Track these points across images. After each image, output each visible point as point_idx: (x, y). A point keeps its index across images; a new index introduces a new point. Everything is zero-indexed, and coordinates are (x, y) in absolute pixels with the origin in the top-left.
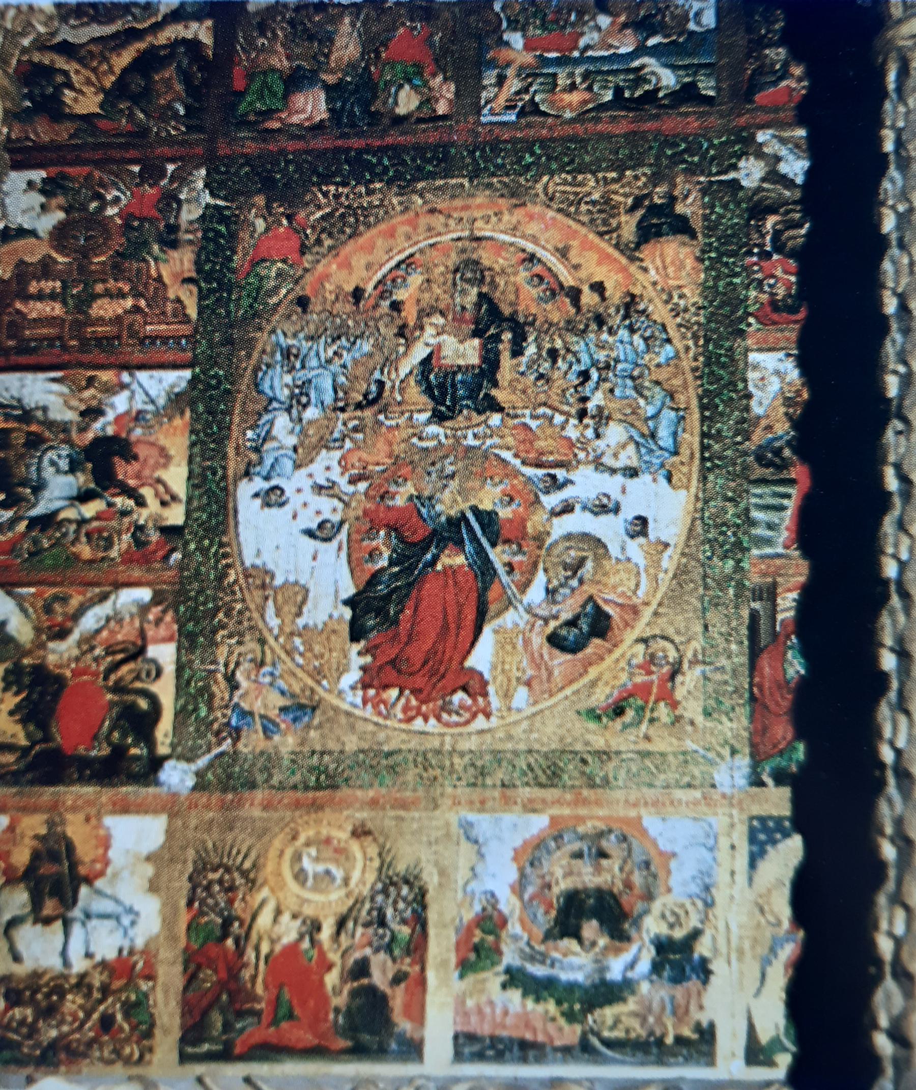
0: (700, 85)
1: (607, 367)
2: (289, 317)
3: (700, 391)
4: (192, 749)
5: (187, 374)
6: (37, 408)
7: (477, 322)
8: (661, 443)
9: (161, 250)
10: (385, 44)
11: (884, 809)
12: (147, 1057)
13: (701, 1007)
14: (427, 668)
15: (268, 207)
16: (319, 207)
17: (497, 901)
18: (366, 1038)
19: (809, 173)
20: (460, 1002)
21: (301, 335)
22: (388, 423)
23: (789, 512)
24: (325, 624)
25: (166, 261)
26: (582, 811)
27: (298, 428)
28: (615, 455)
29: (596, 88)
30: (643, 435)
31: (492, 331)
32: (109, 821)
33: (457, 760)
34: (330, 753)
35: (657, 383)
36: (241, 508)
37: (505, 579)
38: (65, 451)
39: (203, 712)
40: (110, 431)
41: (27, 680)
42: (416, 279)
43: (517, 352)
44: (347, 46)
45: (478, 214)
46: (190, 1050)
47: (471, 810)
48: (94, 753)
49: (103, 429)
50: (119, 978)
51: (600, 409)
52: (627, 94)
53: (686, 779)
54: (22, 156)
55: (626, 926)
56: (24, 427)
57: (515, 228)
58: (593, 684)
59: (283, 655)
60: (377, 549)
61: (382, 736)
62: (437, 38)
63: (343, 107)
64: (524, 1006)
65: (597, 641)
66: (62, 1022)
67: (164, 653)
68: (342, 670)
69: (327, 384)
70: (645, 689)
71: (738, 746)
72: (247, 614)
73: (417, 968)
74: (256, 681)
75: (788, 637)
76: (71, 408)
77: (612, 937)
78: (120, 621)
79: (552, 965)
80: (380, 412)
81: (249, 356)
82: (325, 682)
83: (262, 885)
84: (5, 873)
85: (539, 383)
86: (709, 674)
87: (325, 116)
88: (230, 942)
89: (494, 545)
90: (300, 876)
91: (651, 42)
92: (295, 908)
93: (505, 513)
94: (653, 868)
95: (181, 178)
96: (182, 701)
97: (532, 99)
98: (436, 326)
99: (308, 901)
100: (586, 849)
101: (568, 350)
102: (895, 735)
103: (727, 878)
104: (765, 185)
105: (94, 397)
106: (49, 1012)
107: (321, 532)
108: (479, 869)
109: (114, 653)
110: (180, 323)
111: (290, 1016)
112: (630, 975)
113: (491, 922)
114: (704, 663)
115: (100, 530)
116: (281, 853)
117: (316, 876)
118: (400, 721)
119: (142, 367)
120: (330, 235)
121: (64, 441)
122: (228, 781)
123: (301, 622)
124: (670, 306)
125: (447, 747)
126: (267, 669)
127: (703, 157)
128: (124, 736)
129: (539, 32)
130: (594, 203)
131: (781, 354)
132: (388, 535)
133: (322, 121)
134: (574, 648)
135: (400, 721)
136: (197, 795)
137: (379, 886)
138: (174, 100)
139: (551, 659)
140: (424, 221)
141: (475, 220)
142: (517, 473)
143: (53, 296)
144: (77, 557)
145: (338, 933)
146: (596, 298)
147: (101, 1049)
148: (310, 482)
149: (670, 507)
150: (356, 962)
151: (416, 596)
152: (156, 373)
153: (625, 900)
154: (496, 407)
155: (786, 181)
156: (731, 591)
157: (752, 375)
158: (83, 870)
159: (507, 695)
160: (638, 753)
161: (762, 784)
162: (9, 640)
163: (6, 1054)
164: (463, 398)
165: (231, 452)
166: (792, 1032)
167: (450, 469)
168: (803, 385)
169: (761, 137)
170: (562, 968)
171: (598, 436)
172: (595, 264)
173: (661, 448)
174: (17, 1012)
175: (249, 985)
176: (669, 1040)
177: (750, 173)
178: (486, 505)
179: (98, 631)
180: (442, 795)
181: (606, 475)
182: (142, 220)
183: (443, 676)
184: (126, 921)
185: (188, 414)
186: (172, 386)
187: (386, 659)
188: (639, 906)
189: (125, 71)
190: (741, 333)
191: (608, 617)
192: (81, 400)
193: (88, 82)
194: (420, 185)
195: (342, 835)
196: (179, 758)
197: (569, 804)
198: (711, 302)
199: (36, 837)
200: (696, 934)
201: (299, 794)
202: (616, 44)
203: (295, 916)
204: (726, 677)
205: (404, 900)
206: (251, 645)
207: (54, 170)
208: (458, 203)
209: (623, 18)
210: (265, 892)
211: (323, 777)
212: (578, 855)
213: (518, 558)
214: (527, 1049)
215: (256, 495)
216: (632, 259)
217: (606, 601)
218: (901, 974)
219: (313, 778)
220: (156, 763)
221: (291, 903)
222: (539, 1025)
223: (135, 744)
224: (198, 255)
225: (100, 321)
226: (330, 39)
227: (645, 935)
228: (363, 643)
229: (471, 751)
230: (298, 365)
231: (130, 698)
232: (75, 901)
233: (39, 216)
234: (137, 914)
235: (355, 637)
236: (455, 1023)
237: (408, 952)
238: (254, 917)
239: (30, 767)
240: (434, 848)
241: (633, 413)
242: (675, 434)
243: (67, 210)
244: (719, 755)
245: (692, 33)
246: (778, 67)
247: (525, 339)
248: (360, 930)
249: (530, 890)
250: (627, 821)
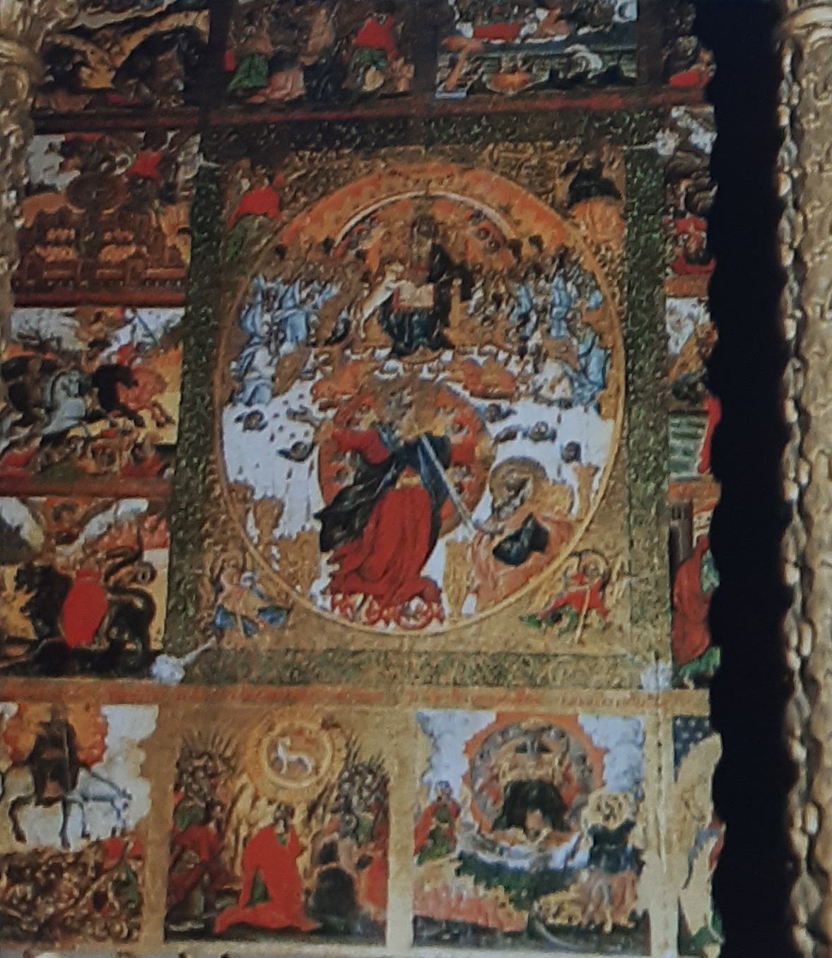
0: (624, 68)
1: (544, 310)
2: (269, 263)
3: (625, 332)
4: (181, 646)
5: (181, 312)
6: (52, 339)
7: (431, 270)
8: (592, 378)
9: (161, 204)
10: (355, 32)
11: (792, 710)
12: (135, 934)
13: (636, 897)
14: (388, 576)
15: (253, 168)
16: (296, 170)
17: (451, 791)
18: (334, 919)
19: (715, 145)
20: (419, 887)
21: (280, 279)
22: (354, 357)
23: (703, 440)
24: (299, 535)
25: (164, 214)
26: (525, 708)
27: (275, 361)
28: (552, 388)
29: (534, 70)
30: (575, 370)
31: (445, 277)
32: (106, 710)
33: (415, 661)
34: (303, 651)
35: (588, 325)
36: (225, 430)
37: (456, 498)
38: (75, 376)
39: (191, 612)
40: (114, 360)
41: (37, 580)
42: (378, 232)
43: (466, 296)
44: (322, 32)
45: (433, 177)
46: (174, 928)
47: (428, 706)
48: (94, 647)
49: (109, 357)
50: (113, 857)
51: (538, 348)
52: (561, 75)
53: (616, 681)
54: (42, 123)
55: (566, 817)
56: (41, 355)
57: (465, 189)
58: (534, 592)
59: (262, 563)
60: (343, 468)
61: (349, 636)
62: (400, 27)
63: (318, 84)
64: (476, 892)
65: (536, 555)
66: (59, 899)
67: (158, 557)
68: (315, 576)
69: (300, 321)
70: (579, 598)
71: (661, 650)
72: (231, 525)
73: (380, 853)
74: (238, 585)
75: (704, 552)
76: (83, 340)
77: (554, 826)
78: (120, 528)
79: (501, 853)
80: (347, 347)
81: (234, 296)
82: (298, 587)
83: (242, 772)
84: (12, 757)
85: (486, 324)
86: (634, 585)
87: (303, 92)
88: (212, 825)
89: (446, 467)
90: (275, 764)
91: (582, 31)
92: (271, 795)
93: (455, 439)
94: (588, 762)
95: (179, 144)
96: (172, 602)
97: (481, 77)
98: (396, 273)
99: (283, 788)
100: (529, 743)
101: (510, 296)
102: (804, 643)
103: (656, 773)
104: (679, 154)
105: (101, 330)
106: (46, 889)
107: (296, 453)
108: (434, 760)
109: (115, 557)
110: (176, 267)
111: (265, 896)
112: (570, 863)
113: (445, 810)
114: (629, 574)
115: (104, 448)
116: (260, 742)
117: (289, 764)
118: (364, 624)
119: (144, 305)
120: (305, 194)
121: (74, 368)
122: (211, 674)
123: (277, 533)
124: (598, 257)
125: (406, 648)
126: (247, 574)
127: (626, 129)
128: (120, 633)
129: (486, 22)
130: (533, 168)
131: (694, 301)
132: (353, 457)
133: (300, 97)
134: (517, 560)
135: (364, 624)
136: (185, 688)
137: (346, 774)
138: (175, 77)
139: (497, 569)
140: (384, 183)
141: (430, 182)
142: (465, 404)
143: (68, 243)
144: (83, 471)
145: (309, 818)
146: (535, 250)
147: (93, 925)
148: (286, 408)
149: (598, 435)
150: (325, 846)
151: (381, 509)
152: (155, 311)
153: (563, 792)
154: (448, 345)
155: (697, 151)
156: (653, 511)
157: (669, 319)
158: (81, 756)
159: (458, 602)
160: (574, 655)
161: (682, 686)
162: (23, 543)
163: (7, 930)
164: (418, 337)
165: (217, 379)
166: (719, 923)
167: (407, 399)
168: (714, 328)
169: (675, 113)
170: (509, 856)
171: (536, 371)
172: (534, 222)
173: (591, 382)
174: (18, 889)
175: (228, 868)
176: (608, 928)
177: (666, 144)
178: (439, 432)
179: (101, 537)
180: (402, 691)
181: (544, 406)
182: (146, 179)
183: (401, 585)
184: (119, 803)
185: (181, 347)
186: (169, 322)
187: (350, 568)
188: (578, 799)
189: (133, 52)
190: (660, 283)
191: (546, 533)
192: (90, 333)
193: (102, 61)
194: (383, 151)
195: (313, 726)
196: (170, 653)
197: (514, 702)
198: (634, 255)
199: (43, 724)
200: (628, 826)
201: (273, 689)
202: (551, 32)
203: (270, 802)
204: (649, 588)
205: (368, 787)
206: (233, 553)
207: (71, 135)
208: (416, 166)
209: (558, 11)
210: (244, 779)
211: (296, 673)
212: (522, 749)
213: (467, 479)
214: (479, 934)
215: (239, 419)
216: (566, 217)
217: (546, 519)
218: (815, 869)
219: (288, 674)
220: (150, 657)
221: (267, 791)
222: (490, 910)
223: (131, 640)
224: (193, 209)
225: (107, 264)
226: (306, 29)
227: (583, 825)
228: (331, 553)
229: (426, 652)
230: (276, 305)
231: (125, 598)
232: (74, 784)
233: (58, 173)
234: (130, 797)
235: (324, 549)
236: (414, 907)
237: (372, 837)
238: (234, 802)
239: (38, 659)
240: (394, 741)
241: (567, 350)
242: (603, 370)
243: (82, 170)
244: (645, 658)
245: (616, 25)
246: (690, 53)
247: (473, 285)
248: (328, 817)
249: (480, 781)
250: (562, 718)
